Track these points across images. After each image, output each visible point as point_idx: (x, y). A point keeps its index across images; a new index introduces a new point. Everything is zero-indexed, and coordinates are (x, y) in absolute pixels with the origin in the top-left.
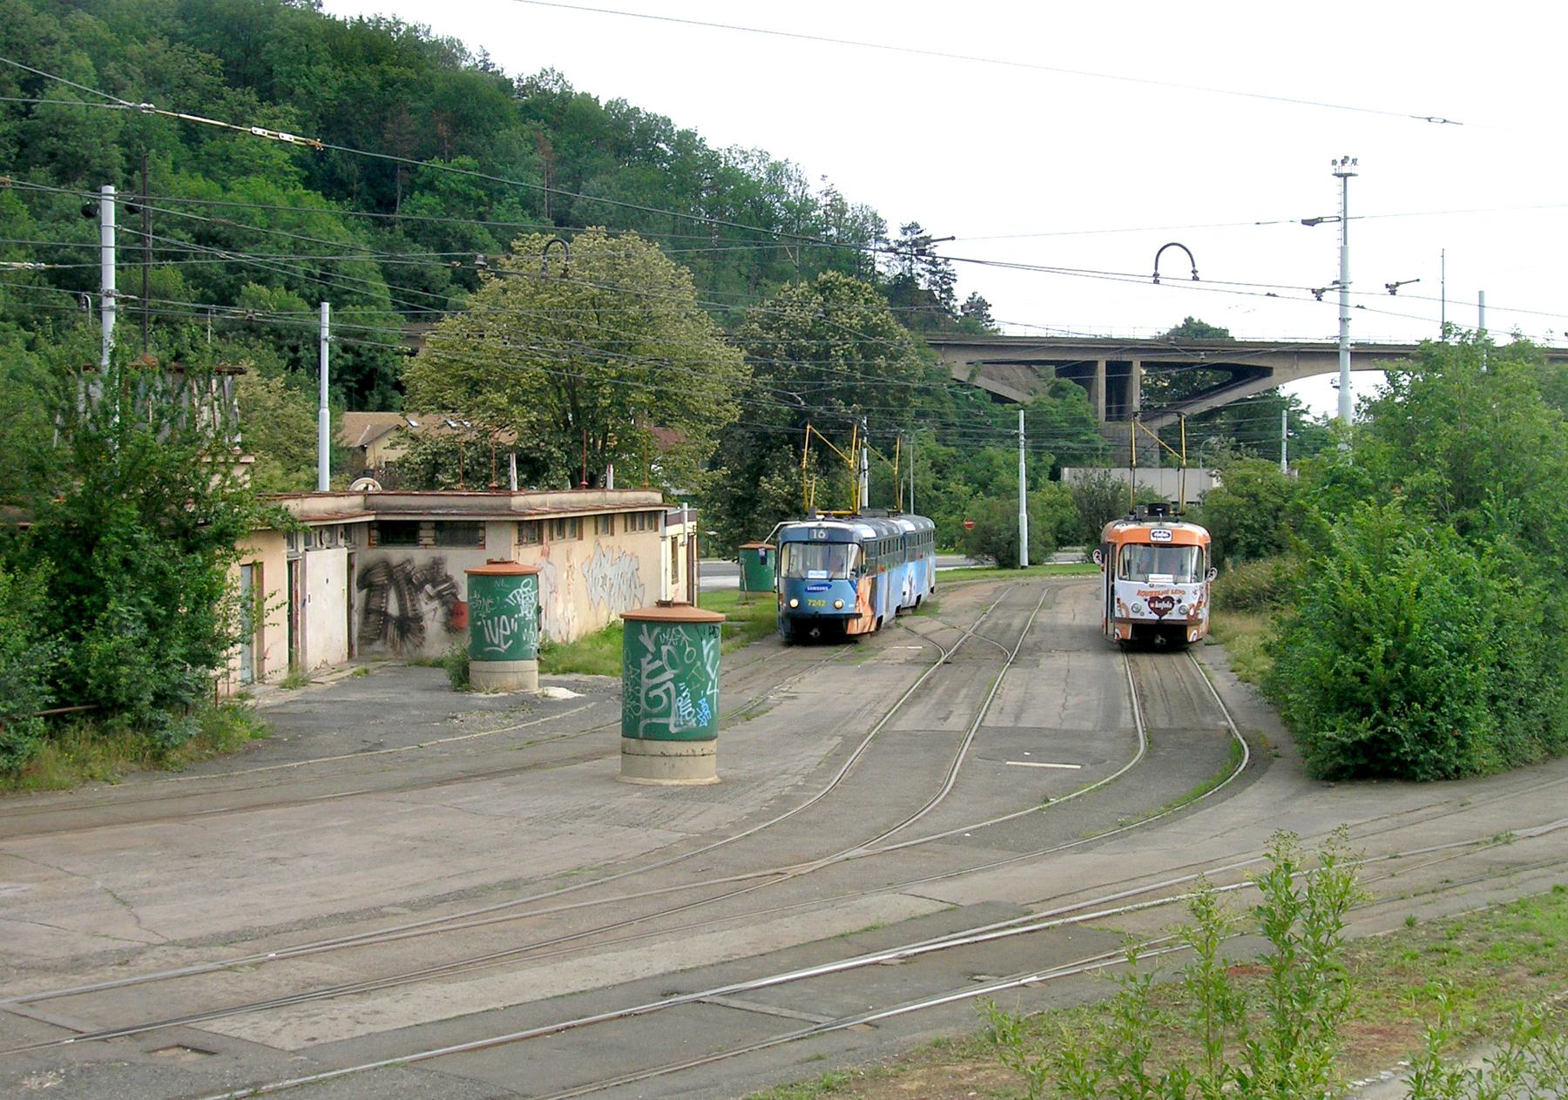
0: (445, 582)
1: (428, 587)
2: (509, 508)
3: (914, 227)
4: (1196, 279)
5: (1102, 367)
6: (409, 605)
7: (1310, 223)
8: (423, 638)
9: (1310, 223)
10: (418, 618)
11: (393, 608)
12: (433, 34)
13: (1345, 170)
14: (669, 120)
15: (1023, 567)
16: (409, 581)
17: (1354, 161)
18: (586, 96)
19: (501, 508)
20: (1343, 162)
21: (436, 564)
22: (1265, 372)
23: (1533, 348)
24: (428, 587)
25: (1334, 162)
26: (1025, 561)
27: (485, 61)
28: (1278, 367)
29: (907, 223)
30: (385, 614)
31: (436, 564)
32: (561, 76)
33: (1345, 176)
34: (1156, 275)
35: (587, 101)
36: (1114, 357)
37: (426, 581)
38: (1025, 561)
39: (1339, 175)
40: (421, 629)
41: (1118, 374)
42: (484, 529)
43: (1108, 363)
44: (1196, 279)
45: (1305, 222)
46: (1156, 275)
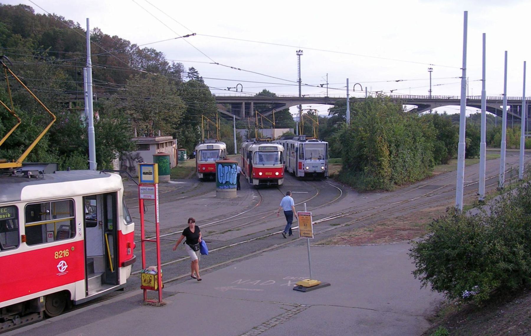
0: (140, 158)
1: (136, 160)
2: (155, 140)
3: (193, 69)
4: (362, 90)
5: (244, 104)
6: (132, 164)
7: (397, 81)
8: (135, 172)
9: (397, 81)
10: (134, 167)
11: (128, 165)
12: (65, 19)
13: (300, 53)
14: (129, 42)
15: (236, 154)
16: (132, 158)
17: (302, 51)
18: (115, 37)
19: (153, 140)
20: (299, 51)
21: (138, 154)
22: (284, 105)
23: (270, 93)
24: (136, 160)
25: (297, 51)
26: (236, 152)
27: (79, 26)
28: (287, 103)
29: (191, 67)
30: (126, 166)
31: (138, 154)
32: (100, 30)
33: (300, 55)
34: (354, 90)
35: (107, 36)
36: (246, 102)
37: (136, 158)
38: (236, 152)
39: (298, 55)
40: (135, 170)
41: (248, 105)
42: (149, 146)
43: (245, 103)
44: (362, 90)
45: (396, 81)
46: (354, 90)
